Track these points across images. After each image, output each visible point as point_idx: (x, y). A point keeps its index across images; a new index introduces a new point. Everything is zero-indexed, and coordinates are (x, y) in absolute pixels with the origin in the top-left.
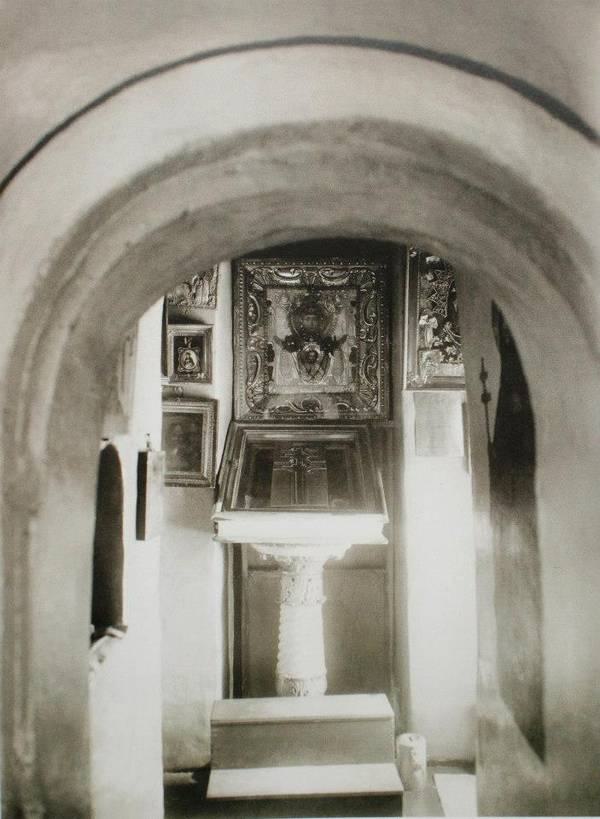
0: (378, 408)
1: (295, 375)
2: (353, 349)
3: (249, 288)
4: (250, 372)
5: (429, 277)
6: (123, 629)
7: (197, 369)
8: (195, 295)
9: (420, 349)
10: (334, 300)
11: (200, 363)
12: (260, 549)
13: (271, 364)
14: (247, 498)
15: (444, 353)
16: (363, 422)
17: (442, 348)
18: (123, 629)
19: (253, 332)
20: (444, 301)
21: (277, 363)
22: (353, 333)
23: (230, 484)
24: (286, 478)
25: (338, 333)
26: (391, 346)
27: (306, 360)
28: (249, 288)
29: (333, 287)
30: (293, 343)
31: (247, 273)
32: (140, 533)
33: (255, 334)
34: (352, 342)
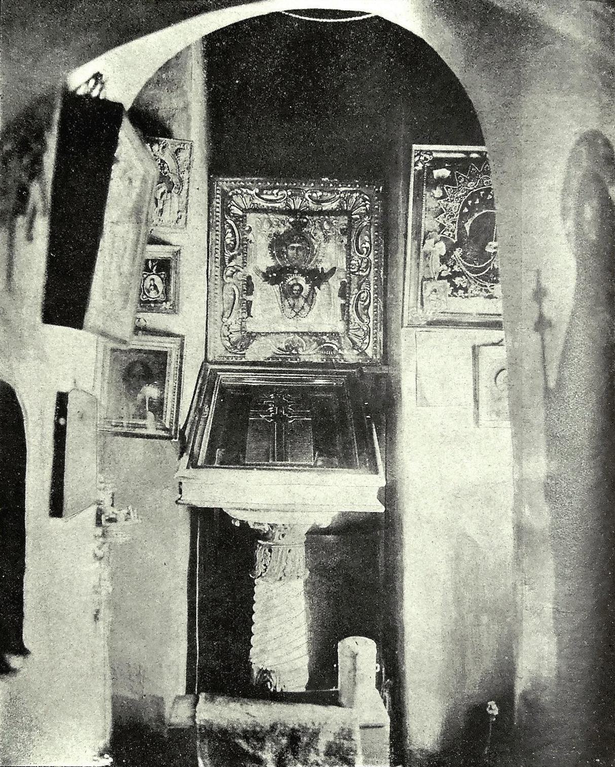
0: (369, 352)
1: (277, 312)
2: (343, 284)
3: (226, 211)
4: (226, 306)
5: (438, 192)
6: (23, 651)
7: (162, 297)
8: (161, 211)
9: (424, 279)
10: (322, 228)
11: (166, 292)
12: (232, 513)
13: (249, 298)
14: (219, 453)
15: (453, 285)
16: (352, 366)
17: (449, 278)
18: (23, 651)
19: (230, 261)
20: (454, 222)
21: (256, 298)
22: (342, 264)
23: (198, 437)
24: (265, 430)
25: (326, 266)
26: (386, 280)
27: (288, 293)
28: (226, 211)
29: (321, 213)
30: (275, 276)
31: (224, 193)
32: (57, 508)
33: (233, 263)
34: (342, 275)
